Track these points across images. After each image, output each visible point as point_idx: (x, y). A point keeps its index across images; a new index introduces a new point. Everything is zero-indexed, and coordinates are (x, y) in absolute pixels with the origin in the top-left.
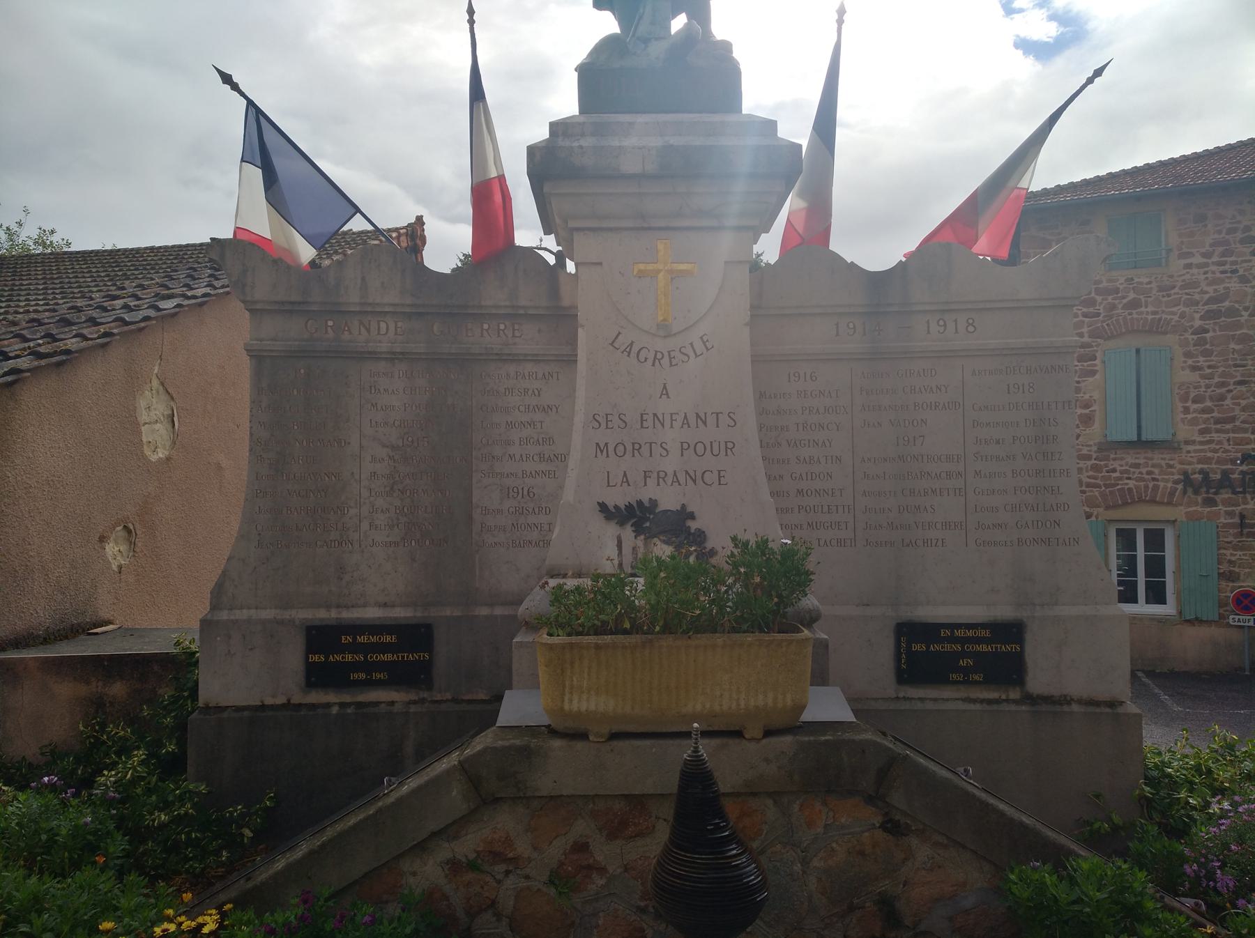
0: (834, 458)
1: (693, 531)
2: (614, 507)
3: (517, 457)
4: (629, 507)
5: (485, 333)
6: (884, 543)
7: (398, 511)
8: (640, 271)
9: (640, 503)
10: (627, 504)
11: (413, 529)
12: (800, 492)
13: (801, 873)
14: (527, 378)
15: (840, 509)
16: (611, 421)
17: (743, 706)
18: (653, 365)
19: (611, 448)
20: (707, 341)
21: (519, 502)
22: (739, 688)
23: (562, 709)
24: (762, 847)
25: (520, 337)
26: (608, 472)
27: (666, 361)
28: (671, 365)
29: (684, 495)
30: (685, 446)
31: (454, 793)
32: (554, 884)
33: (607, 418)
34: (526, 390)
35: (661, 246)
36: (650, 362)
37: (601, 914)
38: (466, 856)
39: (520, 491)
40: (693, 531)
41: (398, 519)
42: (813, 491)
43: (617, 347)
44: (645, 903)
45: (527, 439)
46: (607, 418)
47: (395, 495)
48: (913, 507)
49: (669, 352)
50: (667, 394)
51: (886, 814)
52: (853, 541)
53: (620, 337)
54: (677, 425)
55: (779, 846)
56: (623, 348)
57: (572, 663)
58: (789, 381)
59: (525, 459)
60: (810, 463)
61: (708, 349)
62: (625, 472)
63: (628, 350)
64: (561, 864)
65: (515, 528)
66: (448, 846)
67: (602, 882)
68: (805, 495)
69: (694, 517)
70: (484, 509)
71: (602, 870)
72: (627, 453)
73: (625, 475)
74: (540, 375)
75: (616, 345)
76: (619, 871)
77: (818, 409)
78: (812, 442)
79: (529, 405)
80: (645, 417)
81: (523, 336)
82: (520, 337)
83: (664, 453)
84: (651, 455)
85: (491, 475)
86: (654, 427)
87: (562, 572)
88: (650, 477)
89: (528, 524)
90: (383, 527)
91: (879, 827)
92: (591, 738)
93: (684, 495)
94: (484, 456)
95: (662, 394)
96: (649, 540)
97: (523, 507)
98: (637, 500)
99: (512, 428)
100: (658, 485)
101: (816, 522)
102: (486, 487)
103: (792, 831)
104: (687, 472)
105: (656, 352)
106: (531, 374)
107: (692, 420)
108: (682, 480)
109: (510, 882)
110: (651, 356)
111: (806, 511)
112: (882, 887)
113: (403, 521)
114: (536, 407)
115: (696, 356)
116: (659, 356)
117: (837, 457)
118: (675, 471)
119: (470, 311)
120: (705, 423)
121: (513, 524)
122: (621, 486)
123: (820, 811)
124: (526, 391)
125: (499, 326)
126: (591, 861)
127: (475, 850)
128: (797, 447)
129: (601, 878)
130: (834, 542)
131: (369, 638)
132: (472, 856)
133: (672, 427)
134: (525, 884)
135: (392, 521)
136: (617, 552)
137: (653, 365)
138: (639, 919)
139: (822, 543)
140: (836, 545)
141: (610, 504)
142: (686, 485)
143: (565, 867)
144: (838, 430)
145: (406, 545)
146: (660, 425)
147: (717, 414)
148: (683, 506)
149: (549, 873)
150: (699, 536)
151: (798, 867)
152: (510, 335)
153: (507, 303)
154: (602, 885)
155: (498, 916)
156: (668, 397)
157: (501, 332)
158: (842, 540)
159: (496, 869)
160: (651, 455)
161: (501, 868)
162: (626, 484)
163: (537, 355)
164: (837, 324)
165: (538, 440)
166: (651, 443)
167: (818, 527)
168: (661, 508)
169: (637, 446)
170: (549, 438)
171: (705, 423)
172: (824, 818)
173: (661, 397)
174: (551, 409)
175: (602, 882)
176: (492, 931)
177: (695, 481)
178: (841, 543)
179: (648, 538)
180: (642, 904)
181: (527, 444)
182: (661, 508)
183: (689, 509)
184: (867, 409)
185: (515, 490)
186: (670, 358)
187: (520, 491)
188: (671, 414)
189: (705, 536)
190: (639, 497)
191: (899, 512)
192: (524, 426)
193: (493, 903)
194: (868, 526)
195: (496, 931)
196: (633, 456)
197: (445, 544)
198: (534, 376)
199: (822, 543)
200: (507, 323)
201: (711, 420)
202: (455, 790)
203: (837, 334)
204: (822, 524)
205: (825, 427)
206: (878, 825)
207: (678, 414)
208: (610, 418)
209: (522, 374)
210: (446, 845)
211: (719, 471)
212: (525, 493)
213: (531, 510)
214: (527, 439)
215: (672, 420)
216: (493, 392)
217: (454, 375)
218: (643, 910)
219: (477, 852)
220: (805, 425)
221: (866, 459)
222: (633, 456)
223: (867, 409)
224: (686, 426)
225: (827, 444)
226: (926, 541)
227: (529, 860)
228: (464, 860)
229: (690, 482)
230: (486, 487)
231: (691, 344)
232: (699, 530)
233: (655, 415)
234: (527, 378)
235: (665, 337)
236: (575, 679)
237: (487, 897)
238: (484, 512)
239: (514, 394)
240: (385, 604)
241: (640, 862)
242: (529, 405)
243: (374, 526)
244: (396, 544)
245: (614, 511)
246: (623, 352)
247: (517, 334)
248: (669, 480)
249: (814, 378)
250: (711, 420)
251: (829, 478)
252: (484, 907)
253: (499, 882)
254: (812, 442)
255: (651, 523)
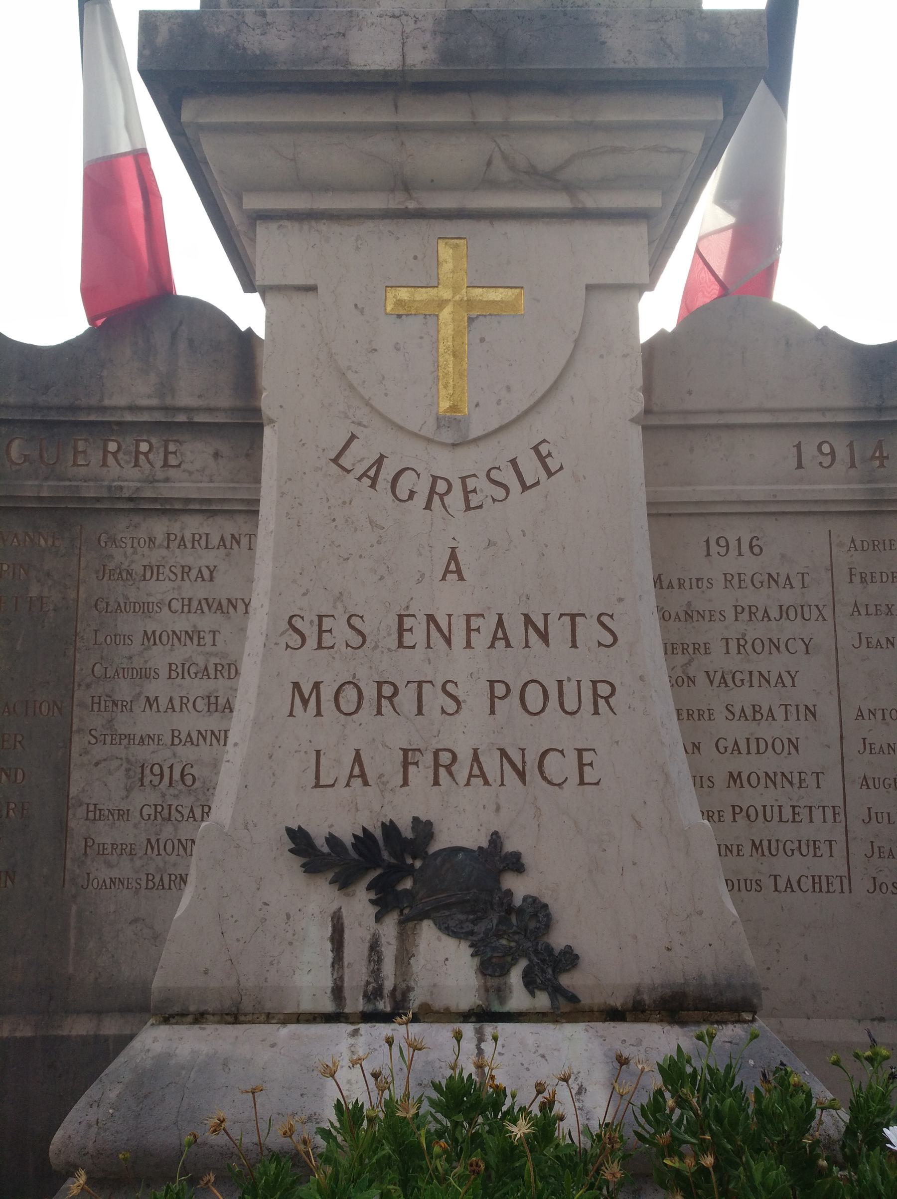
0: (802, 709)
1: (518, 901)
2: (327, 840)
3: (163, 702)
4: (365, 840)
5: (110, 459)
8: (399, 303)
9: (390, 829)
10: (360, 833)
12: (734, 778)
14: (189, 545)
15: (817, 814)
16: (330, 631)
18: (428, 507)
19: (327, 694)
20: (549, 455)
21: (163, 795)
25: (179, 466)
26: (318, 753)
27: (456, 499)
28: (468, 508)
29: (498, 809)
30: (500, 690)
33: (320, 625)
34: (186, 570)
35: (445, 252)
36: (420, 500)
39: (167, 772)
40: (518, 901)
42: (762, 776)
43: (349, 468)
45: (183, 665)
46: (320, 625)
49: (463, 479)
50: (459, 572)
52: (845, 882)
53: (355, 443)
54: (481, 640)
56: (359, 471)
58: (708, 555)
59: (177, 708)
60: (754, 719)
61: (550, 474)
62: (358, 753)
63: (372, 473)
65: (152, 848)
68: (745, 783)
69: (523, 865)
70: (91, 808)
72: (365, 704)
73: (358, 758)
74: (215, 541)
75: (345, 461)
77: (766, 611)
78: (756, 675)
79: (190, 600)
80: (408, 623)
81: (183, 466)
82: (179, 466)
83: (451, 707)
84: (420, 712)
85: (108, 739)
86: (429, 646)
87: (192, 1008)
88: (416, 764)
89: (179, 840)
93: (498, 809)
94: (96, 700)
95: (447, 571)
96: (410, 925)
97: (170, 806)
98: (383, 824)
99: (155, 644)
100: (436, 783)
101: (769, 841)
102: (97, 764)
104: (504, 753)
105: (435, 479)
106: (197, 537)
107: (516, 629)
108: (492, 772)
110: (423, 489)
111: (748, 816)
114: (203, 602)
115: (525, 487)
116: (441, 487)
117: (807, 707)
118: (476, 751)
119: (83, 417)
120: (544, 637)
121: (149, 841)
122: (348, 785)
124: (186, 570)
125: (137, 446)
128: (727, 686)
130: (807, 884)
133: (469, 645)
136: (331, 955)
137: (428, 507)
139: (782, 884)
140: (811, 889)
141: (318, 833)
142: (502, 784)
144: (807, 652)
146: (442, 641)
147: (573, 617)
148: (496, 839)
150: (535, 915)
152: (159, 463)
153: (154, 402)
156: (461, 578)
157: (142, 457)
158: (824, 880)
160: (420, 712)
162: (359, 781)
163: (209, 501)
164: (798, 446)
165: (206, 668)
166: (420, 684)
167: (774, 852)
168: (443, 841)
169: (387, 690)
170: (229, 665)
171: (544, 637)
173: (444, 578)
174: (235, 608)
177: (522, 775)
178: (819, 883)
179: (408, 919)
181: (183, 677)
182: (443, 841)
183: (510, 847)
184: (863, 612)
185: (156, 769)
186: (466, 493)
187: (167, 772)
188: (468, 617)
189: (548, 916)
190: (390, 815)
192: (179, 640)
194: (876, 850)
196: (379, 712)
197: (9, 883)
198: (203, 543)
199: (782, 884)
200: (154, 441)
201: (559, 630)
203: (800, 466)
204: (781, 847)
205: (782, 648)
207: (482, 615)
208: (327, 624)
209: (179, 538)
211: (580, 752)
212: (177, 776)
213: (186, 812)
214: (183, 665)
215: (469, 630)
216: (120, 573)
217: (46, 541)
220: (742, 642)
221: (866, 714)
222: (379, 712)
223: (863, 612)
224: (500, 644)
225: (788, 680)
229: (510, 775)
230: (97, 764)
231: (514, 462)
232: (535, 900)
233: (431, 618)
234: (189, 545)
235: (454, 445)
238: (91, 815)
239: (161, 577)
242: (190, 600)
245: (326, 849)
246: (359, 479)
247: (172, 460)
248: (462, 771)
249: (756, 550)
250: (559, 630)
251: (793, 750)
254: (756, 675)
255: (415, 882)
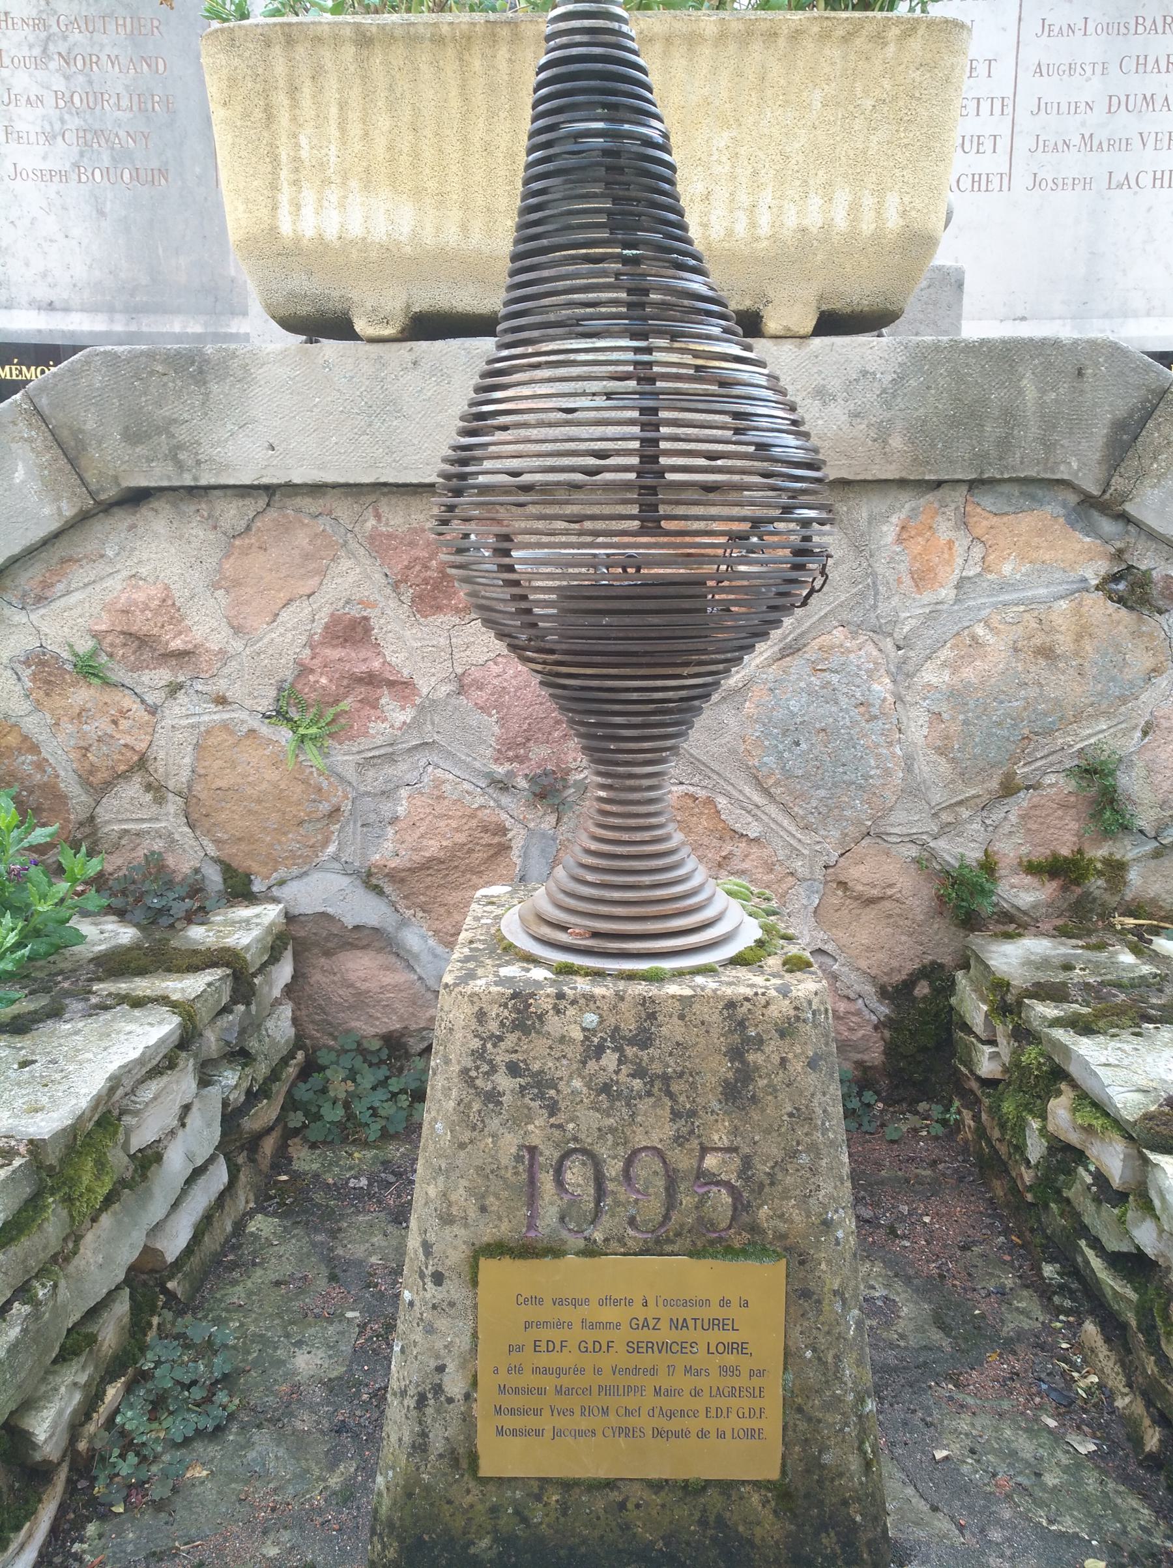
6: (1070, 181)
7: (61, 103)
11: (95, 146)
13: (891, 699)
17: (764, 230)
22: (755, 173)
23: (273, 230)
24: (799, 631)
31: (20, 475)
32: (289, 720)
37: (404, 792)
38: (71, 646)
41: (63, 121)
44: (507, 767)
47: (53, 65)
48: (1140, 97)
51: (1119, 555)
55: (839, 633)
57: (293, 91)
64: (304, 670)
66: (24, 620)
67: (405, 716)
71: (402, 687)
76: (445, 689)
90: (33, 139)
91: (1097, 588)
92: (360, 326)
103: (876, 594)
109: (178, 711)
112: (1090, 736)
113: (74, 128)
123: (950, 543)
126: (376, 664)
127: (90, 631)
129: (403, 708)
131: (21, 372)
132: (84, 646)
134: (216, 717)
135: (51, 124)
138: (492, 803)
140: (970, 188)
143: (312, 678)
145: (84, 178)
149: (273, 693)
151: (882, 687)
154: (404, 723)
155: (157, 790)
158: (984, 178)
159: (145, 679)
161: (163, 675)
172: (960, 561)
175: (405, 716)
176: (145, 826)
180: (501, 770)
191: (1110, 112)
193: (142, 763)
194: (1041, 143)
195: (157, 825)
202: (20, 467)
206: (1094, 582)
210: (20, 617)
218: (503, 785)
219: (95, 635)
226: (1159, 175)
227: (224, 656)
228: (65, 655)
236: (303, 141)
237: (126, 746)
240: (51, 304)
241: (496, 669)
243: (15, 135)
244: (63, 176)
252: (123, 768)
253: (153, 710)
